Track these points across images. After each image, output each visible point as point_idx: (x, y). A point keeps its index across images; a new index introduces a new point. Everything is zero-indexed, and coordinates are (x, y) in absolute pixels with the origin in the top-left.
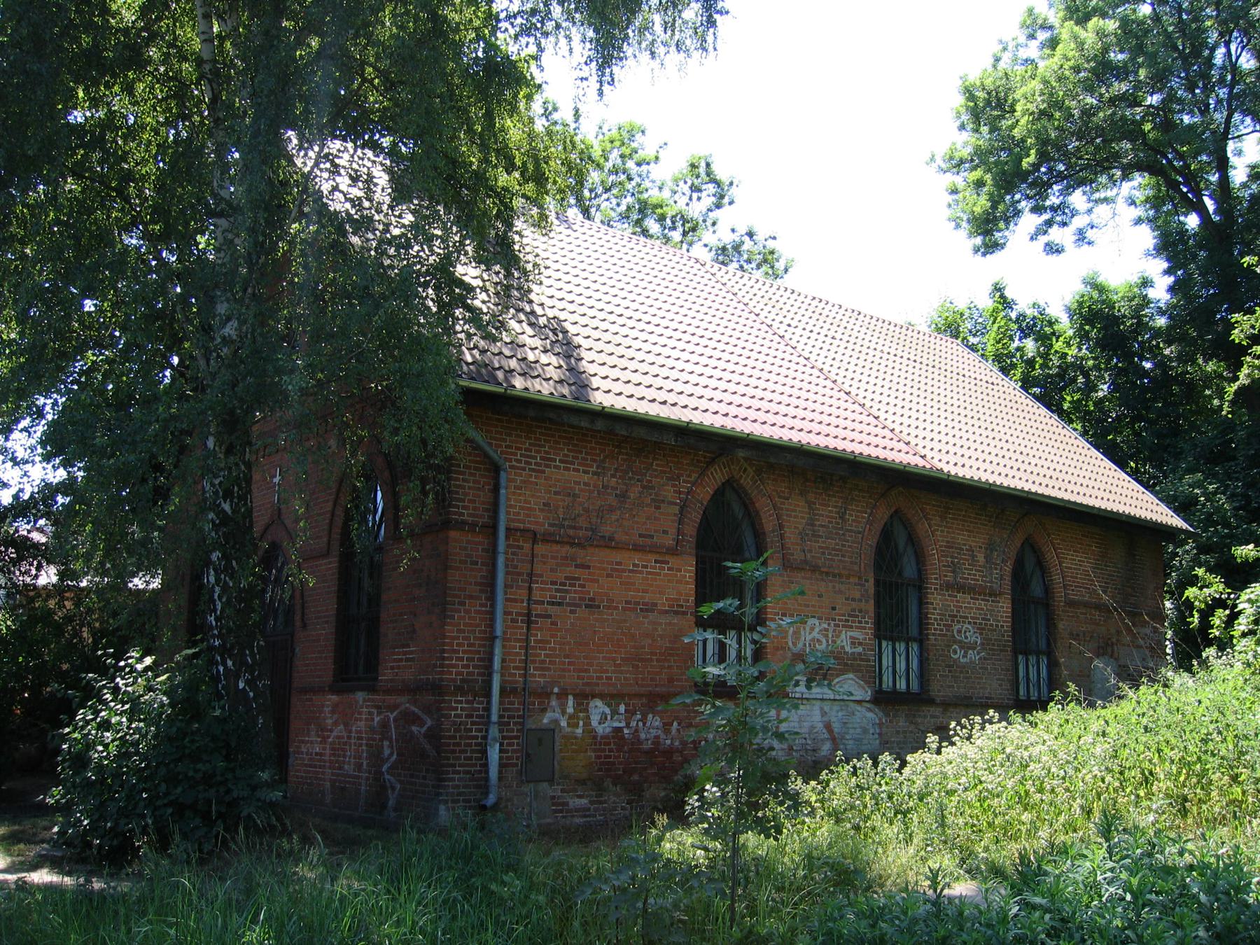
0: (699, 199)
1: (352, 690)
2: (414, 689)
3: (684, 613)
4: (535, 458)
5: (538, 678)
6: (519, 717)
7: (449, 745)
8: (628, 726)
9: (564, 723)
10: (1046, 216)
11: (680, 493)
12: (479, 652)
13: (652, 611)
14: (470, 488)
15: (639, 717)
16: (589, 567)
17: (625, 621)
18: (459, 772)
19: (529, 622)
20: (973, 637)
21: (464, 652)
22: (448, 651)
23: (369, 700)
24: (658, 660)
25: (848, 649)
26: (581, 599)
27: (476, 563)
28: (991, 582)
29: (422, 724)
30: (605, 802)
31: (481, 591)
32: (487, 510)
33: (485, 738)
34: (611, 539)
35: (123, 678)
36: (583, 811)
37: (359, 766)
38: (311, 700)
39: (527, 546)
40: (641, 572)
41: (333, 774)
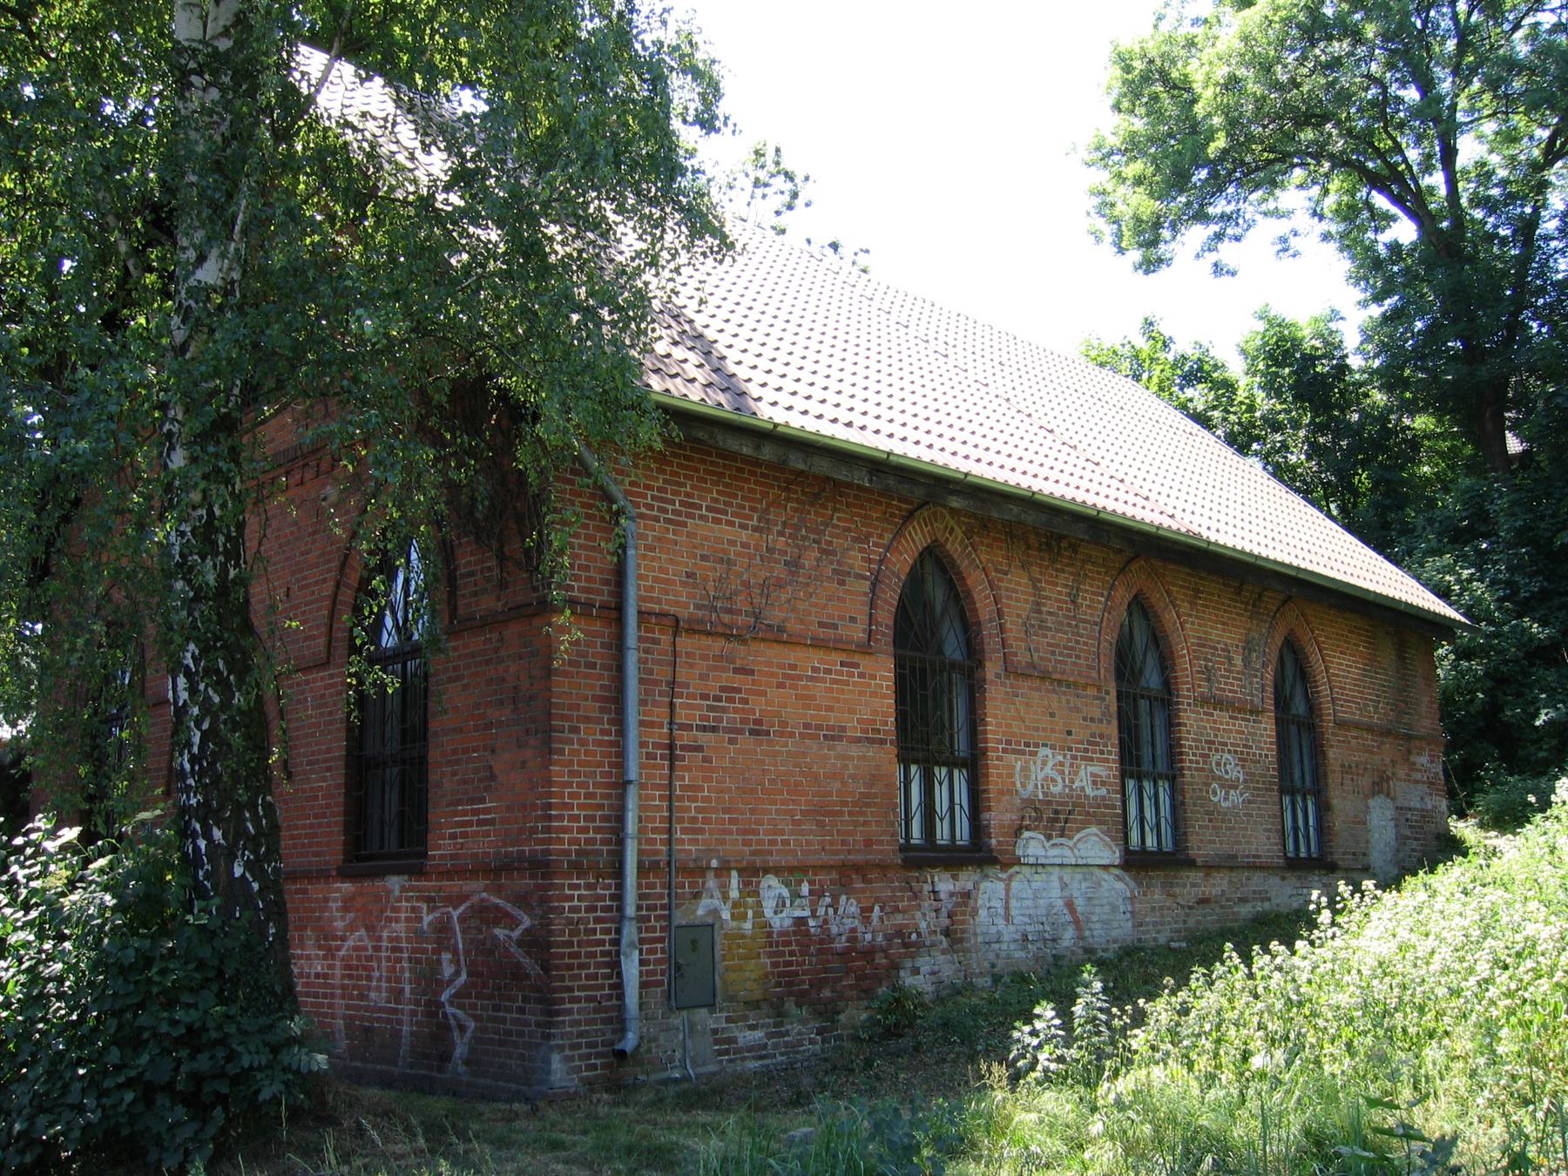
0: (764, 196)
1: (382, 873)
2: (496, 870)
3: (883, 742)
4: (673, 502)
5: (688, 847)
6: (663, 907)
7: (562, 956)
8: (814, 915)
9: (726, 915)
10: (1214, 228)
11: (870, 561)
12: (601, 807)
13: (840, 738)
14: (581, 547)
15: (828, 900)
16: (752, 672)
17: (804, 754)
18: (577, 1000)
19: (672, 758)
20: (1234, 772)
21: (581, 807)
22: (556, 807)
23: (412, 889)
24: (851, 813)
25: (1089, 791)
26: (743, 721)
27: (593, 665)
28: (1251, 694)
29: (513, 923)
30: (787, 1033)
31: (602, 710)
32: (606, 582)
33: (617, 942)
34: (781, 629)
35: (23, 867)
36: (758, 1050)
37: (397, 994)
38: (305, 891)
39: (666, 638)
40: (823, 680)
41: (348, 1007)
